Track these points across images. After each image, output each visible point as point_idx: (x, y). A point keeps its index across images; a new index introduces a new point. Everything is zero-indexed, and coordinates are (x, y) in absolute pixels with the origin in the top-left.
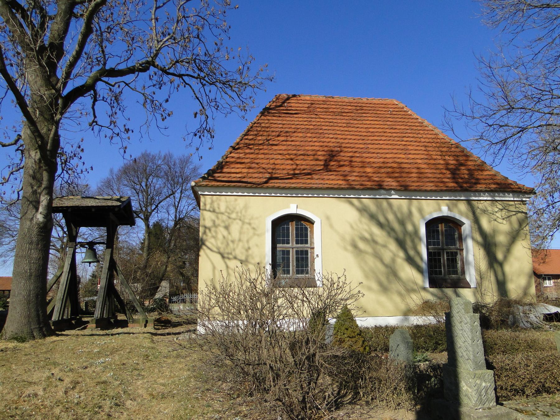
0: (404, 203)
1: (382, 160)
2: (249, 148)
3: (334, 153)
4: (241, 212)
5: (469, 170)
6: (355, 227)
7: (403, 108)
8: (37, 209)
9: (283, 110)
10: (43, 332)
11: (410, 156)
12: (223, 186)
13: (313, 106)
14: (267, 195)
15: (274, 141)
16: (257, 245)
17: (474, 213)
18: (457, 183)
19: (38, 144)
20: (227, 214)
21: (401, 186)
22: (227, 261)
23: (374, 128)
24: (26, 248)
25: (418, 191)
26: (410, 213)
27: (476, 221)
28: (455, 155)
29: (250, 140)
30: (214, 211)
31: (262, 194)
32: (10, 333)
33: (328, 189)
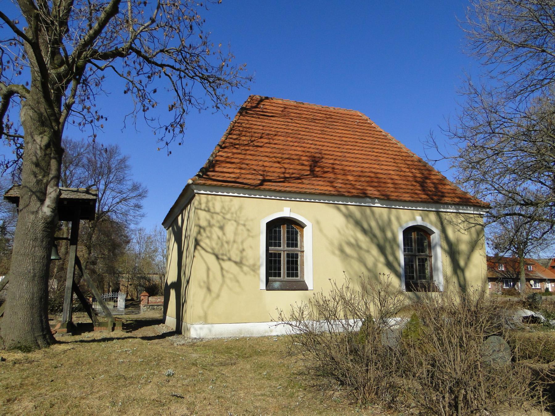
0: (385, 211)
1: (359, 169)
2: (235, 148)
3: (317, 159)
4: (236, 214)
5: (434, 183)
6: (342, 232)
7: (367, 120)
8: (42, 201)
9: (259, 111)
10: (47, 340)
11: (383, 167)
12: (221, 186)
13: (286, 110)
14: (263, 197)
15: (258, 142)
16: (251, 247)
17: (442, 223)
18: (427, 195)
19: (54, 129)
20: (222, 214)
21: (383, 195)
22: (221, 262)
23: (346, 137)
24: (29, 245)
25: (283, 192)
26: (390, 221)
27: (444, 231)
28: (420, 169)
29: (235, 139)
30: (209, 211)
31: (258, 196)
32: (10, 341)
33: (320, 194)
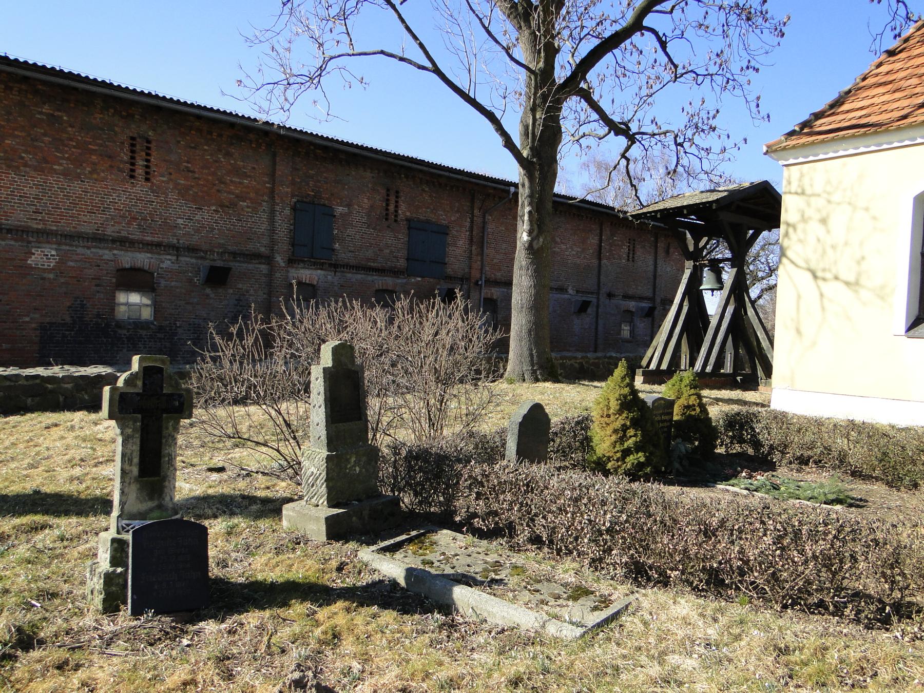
22: (820, 282)
